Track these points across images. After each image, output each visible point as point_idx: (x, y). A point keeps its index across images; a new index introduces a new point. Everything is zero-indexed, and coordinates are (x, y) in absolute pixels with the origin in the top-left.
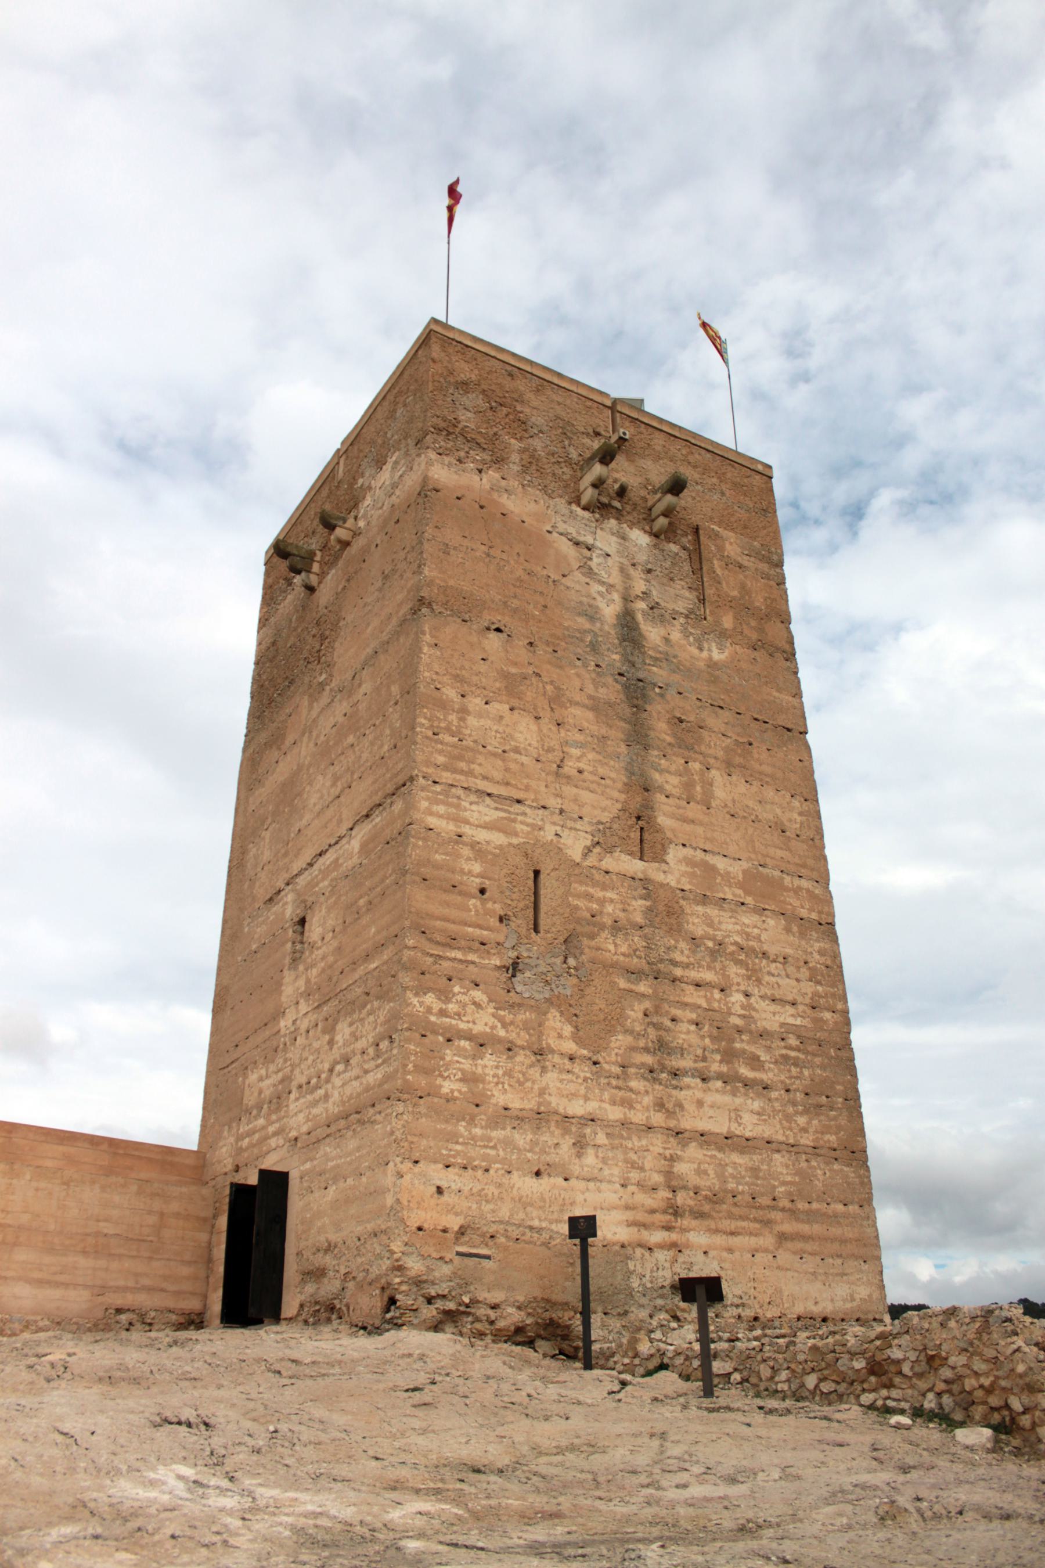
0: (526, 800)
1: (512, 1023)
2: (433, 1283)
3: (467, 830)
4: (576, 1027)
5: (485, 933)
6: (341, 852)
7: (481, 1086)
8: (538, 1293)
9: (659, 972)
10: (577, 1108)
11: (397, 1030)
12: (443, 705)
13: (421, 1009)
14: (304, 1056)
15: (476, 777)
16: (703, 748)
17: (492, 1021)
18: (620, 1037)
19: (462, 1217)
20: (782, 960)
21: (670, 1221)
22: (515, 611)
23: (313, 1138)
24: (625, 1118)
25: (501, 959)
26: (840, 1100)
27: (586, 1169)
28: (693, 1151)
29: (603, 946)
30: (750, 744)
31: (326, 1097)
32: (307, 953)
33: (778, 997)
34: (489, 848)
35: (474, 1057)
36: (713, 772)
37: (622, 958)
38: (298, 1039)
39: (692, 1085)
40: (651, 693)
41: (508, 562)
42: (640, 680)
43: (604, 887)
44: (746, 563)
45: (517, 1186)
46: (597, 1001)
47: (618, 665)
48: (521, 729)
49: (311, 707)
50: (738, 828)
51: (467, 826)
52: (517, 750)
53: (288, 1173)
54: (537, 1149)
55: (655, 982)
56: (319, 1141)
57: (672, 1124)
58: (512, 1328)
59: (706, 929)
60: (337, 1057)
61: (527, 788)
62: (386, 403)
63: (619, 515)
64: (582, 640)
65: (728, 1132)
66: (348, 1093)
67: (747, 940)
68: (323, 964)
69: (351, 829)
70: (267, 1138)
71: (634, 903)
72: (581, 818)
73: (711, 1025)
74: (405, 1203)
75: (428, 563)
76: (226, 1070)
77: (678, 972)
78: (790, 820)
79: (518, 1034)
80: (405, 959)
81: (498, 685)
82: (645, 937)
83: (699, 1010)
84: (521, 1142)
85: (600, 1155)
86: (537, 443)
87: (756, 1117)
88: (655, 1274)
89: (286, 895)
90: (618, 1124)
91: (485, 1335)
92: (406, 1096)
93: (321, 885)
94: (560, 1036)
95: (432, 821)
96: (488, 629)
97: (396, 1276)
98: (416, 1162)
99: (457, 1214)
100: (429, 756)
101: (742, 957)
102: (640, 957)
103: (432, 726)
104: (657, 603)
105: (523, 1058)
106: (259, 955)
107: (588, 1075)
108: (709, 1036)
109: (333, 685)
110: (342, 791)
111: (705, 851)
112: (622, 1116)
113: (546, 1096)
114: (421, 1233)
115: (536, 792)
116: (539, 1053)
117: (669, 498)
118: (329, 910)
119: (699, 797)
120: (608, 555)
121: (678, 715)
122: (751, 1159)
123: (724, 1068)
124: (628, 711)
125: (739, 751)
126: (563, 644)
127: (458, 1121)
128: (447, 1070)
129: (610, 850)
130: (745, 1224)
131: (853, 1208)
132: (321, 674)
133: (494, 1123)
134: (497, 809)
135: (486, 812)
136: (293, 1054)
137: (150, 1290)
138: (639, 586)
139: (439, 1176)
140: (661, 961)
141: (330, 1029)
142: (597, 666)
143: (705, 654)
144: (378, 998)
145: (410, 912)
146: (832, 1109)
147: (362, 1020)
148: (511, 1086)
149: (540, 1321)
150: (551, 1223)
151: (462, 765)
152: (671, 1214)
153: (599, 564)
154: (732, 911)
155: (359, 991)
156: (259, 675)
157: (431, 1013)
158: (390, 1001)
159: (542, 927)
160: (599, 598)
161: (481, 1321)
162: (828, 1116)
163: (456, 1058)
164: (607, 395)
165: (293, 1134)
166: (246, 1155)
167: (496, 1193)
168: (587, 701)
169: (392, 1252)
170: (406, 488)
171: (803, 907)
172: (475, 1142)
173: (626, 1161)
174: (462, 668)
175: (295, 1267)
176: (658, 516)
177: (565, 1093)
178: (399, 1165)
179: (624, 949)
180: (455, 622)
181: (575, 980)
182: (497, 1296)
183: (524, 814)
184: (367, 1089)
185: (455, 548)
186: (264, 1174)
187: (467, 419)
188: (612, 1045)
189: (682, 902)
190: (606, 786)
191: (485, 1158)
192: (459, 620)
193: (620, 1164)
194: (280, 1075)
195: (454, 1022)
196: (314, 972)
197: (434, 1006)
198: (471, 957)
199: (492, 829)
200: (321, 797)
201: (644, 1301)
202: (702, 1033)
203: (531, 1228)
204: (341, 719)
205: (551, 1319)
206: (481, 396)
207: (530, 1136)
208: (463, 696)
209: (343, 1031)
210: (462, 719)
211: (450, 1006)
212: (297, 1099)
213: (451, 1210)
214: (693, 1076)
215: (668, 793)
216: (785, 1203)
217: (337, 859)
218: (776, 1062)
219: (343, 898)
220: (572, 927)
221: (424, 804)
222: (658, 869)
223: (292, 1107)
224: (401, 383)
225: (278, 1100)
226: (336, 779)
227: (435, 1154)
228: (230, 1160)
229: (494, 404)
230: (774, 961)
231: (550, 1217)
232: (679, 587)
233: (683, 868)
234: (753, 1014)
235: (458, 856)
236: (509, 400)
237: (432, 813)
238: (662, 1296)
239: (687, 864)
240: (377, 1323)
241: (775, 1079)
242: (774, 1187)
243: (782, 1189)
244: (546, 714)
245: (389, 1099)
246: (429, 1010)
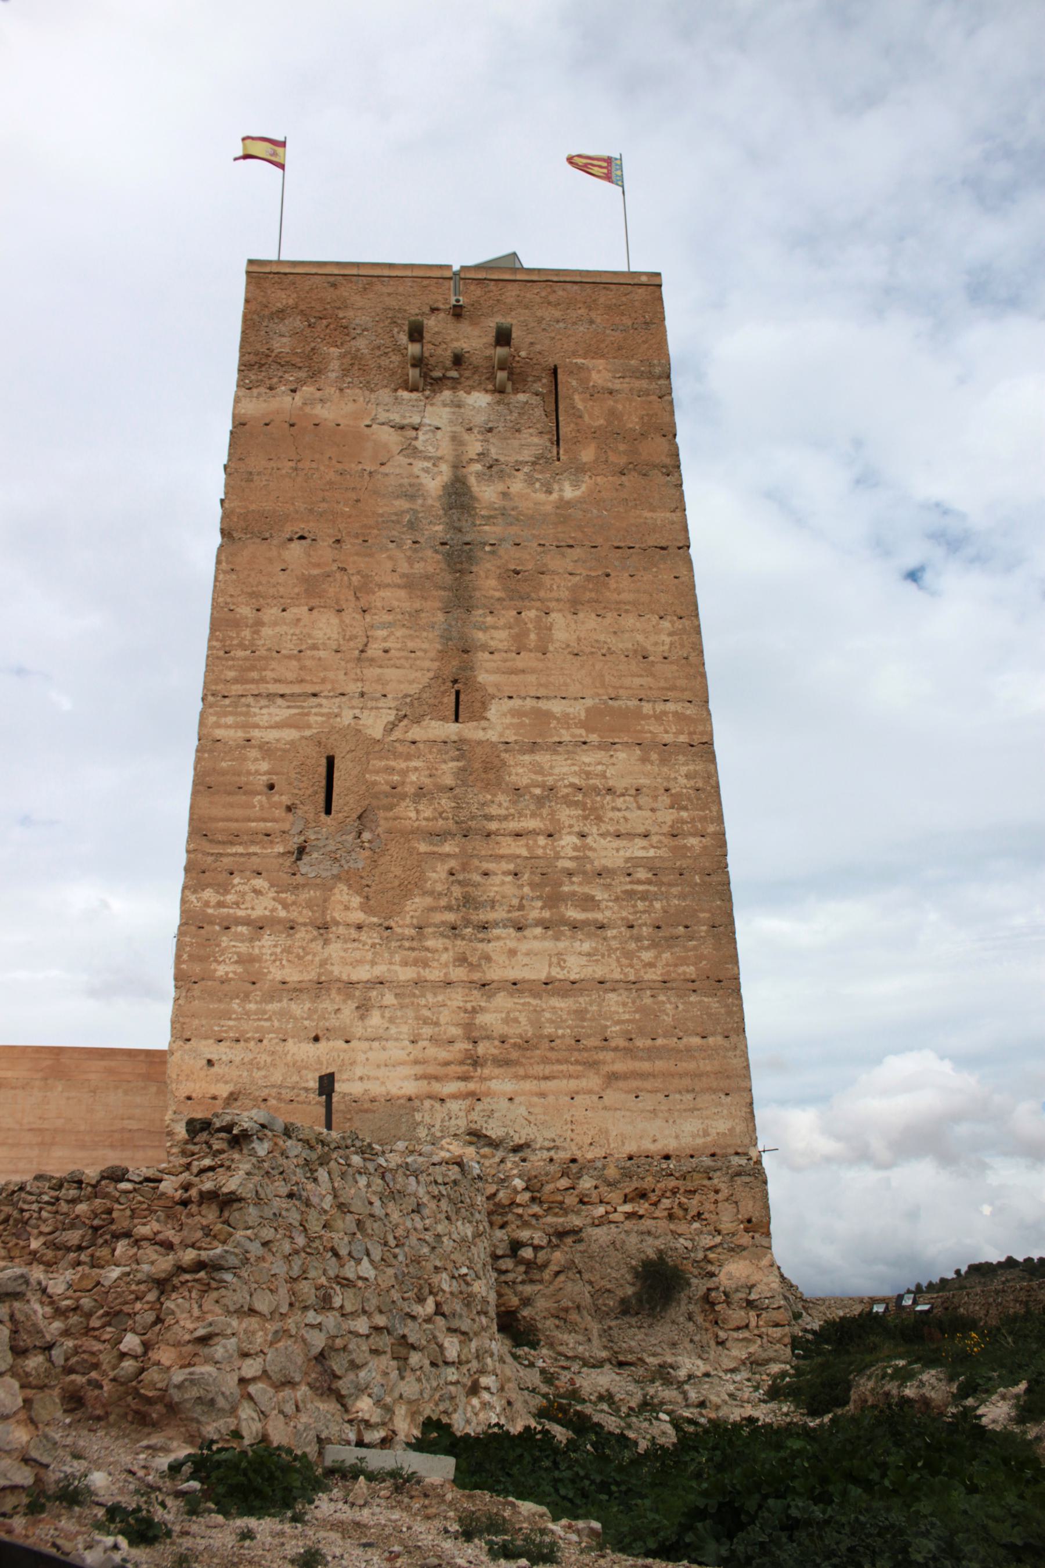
134: (289, 707)
151: (254, 675)
174: (260, 583)
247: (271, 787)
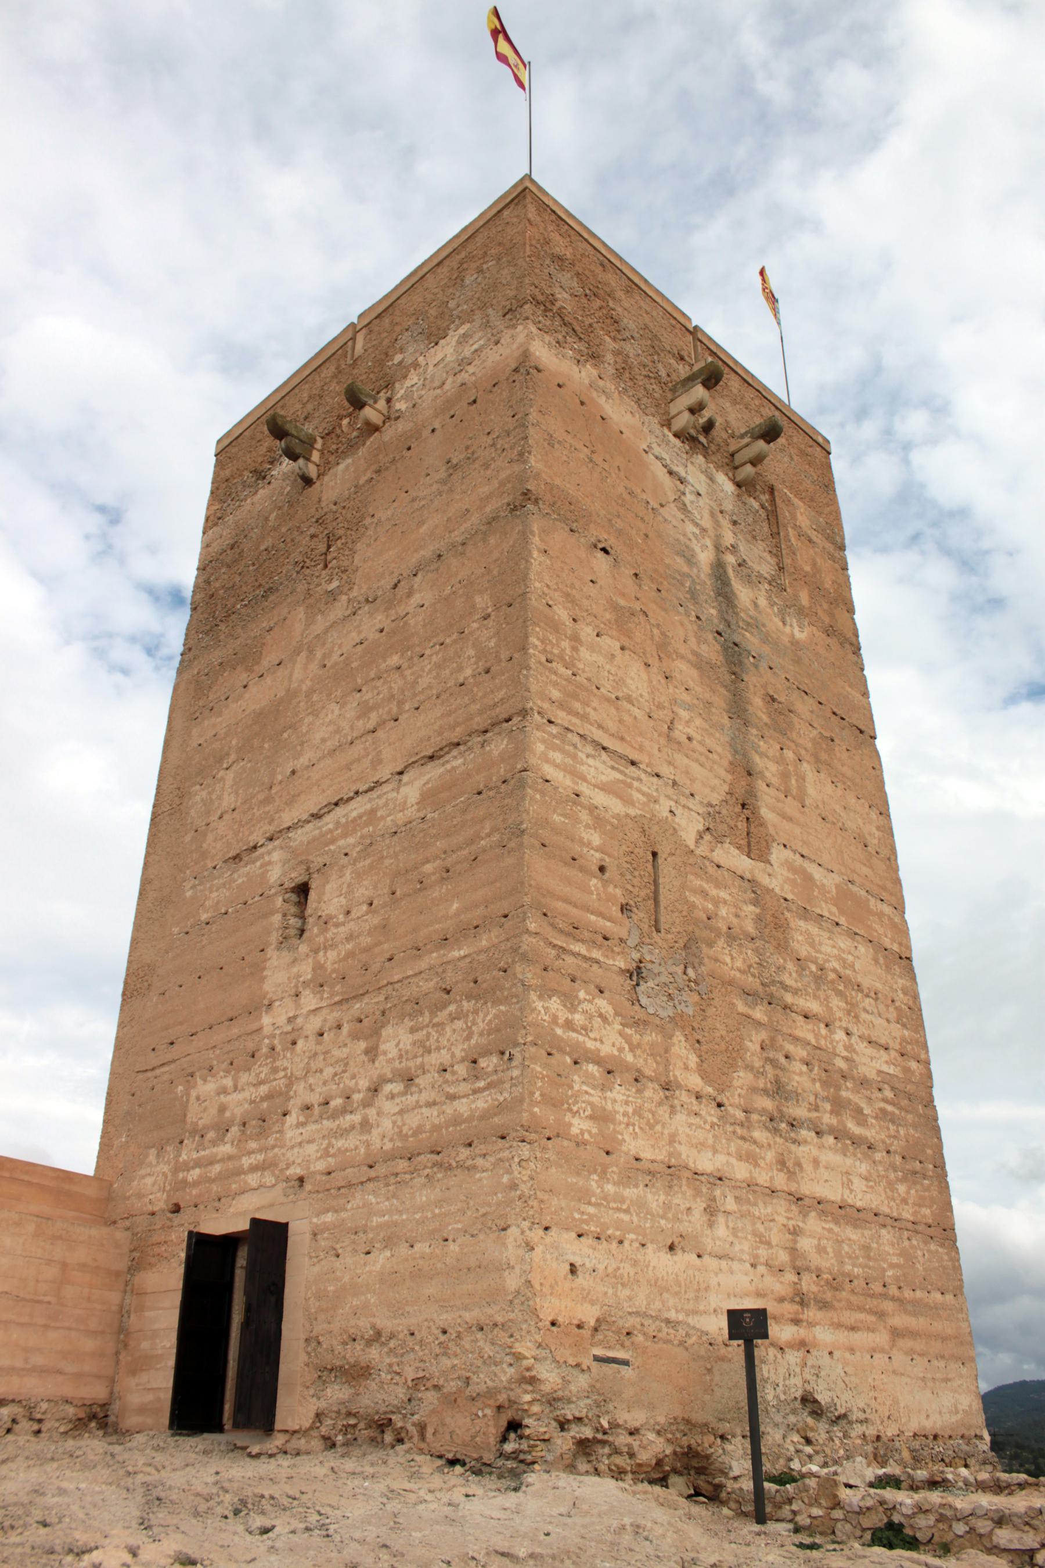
0: (640, 763)
1: (639, 1045)
2: (569, 1401)
3: (583, 788)
4: (699, 1056)
5: (608, 924)
7: (612, 1127)
8: (678, 1412)
9: (771, 995)
10: (706, 1163)
11: (516, 1044)
12: (555, 627)
13: (546, 1018)
14: (314, 1066)
15: (591, 724)
16: (794, 736)
17: (620, 1041)
18: (741, 1074)
19: (598, 1307)
20: (873, 995)
21: (797, 1313)
22: (620, 532)
23: (338, 1178)
24: (751, 1178)
25: (625, 961)
26: (931, 1166)
27: (718, 1243)
28: (813, 1223)
29: (720, 957)
30: (833, 740)
31: (365, 1126)
33: (874, 1039)
34: (608, 816)
35: (604, 1088)
36: (805, 765)
37: (738, 974)
38: (300, 1043)
39: (809, 1139)
40: (746, 661)
41: (610, 473)
42: (736, 644)
43: (718, 885)
44: (814, 539)
45: (652, 1264)
46: (718, 1026)
47: (716, 621)
48: (633, 674)
49: (310, 621)
50: (829, 834)
51: (580, 782)
52: (629, 700)
53: (287, 1224)
54: (670, 1215)
55: (770, 1008)
56: (350, 1185)
57: (793, 1187)
58: (654, 1462)
59: (809, 949)
61: (641, 749)
62: (443, 270)
63: (706, 452)
64: (683, 585)
65: (843, 1200)
67: (844, 967)
69: (401, 773)
70: (239, 1172)
71: (745, 908)
72: (692, 795)
73: (819, 1066)
74: (537, 1287)
75: (534, 452)
76: (149, 1074)
77: (789, 998)
78: (870, 834)
79: (646, 1060)
80: (524, 947)
81: (608, 616)
82: (756, 951)
83: (808, 1047)
84: (654, 1205)
85: (731, 1225)
86: (629, 348)
87: (865, 1183)
88: (787, 1382)
90: (745, 1185)
91: (625, 1472)
92: (533, 1136)
94: (686, 1068)
95: (549, 771)
96: (595, 546)
97: (526, 1392)
98: (546, 1229)
99: (593, 1303)
100: (543, 687)
101: (841, 988)
102: (753, 976)
103: (545, 650)
104: (744, 561)
105: (652, 1092)
106: (214, 927)
107: (715, 1120)
108: (820, 1080)
109: (354, 593)
110: (382, 723)
111: (802, 856)
112: (748, 1175)
113: (676, 1145)
114: (554, 1329)
115: (650, 755)
116: (666, 1087)
117: (761, 444)
118: (359, 876)
119: (794, 792)
120: (699, 494)
121: (772, 693)
122: (863, 1235)
123: (834, 1121)
124: (728, 678)
125: (824, 746)
127: (590, 1173)
128: (575, 1103)
129: (719, 840)
130: (862, 1316)
131: (949, 1297)
132: (331, 581)
133: (626, 1180)
134: (613, 768)
135: (600, 769)
136: (293, 1062)
137: (42, 1371)
138: (729, 538)
139: (582, 1252)
140: (773, 982)
142: (698, 617)
143: (788, 629)
144: (469, 997)
145: (530, 886)
146: (925, 1177)
147: (440, 1026)
148: (641, 1128)
149: (678, 1449)
150: (688, 1315)
152: (798, 1303)
153: (692, 502)
154: (830, 931)
155: (427, 985)
156: (208, 582)
157: (557, 1024)
158: (497, 1002)
159: (663, 926)
160: (694, 541)
161: (620, 1453)
162: (922, 1185)
163: (585, 1088)
164: (689, 319)
167: (632, 1274)
168: (690, 657)
169: (519, 1357)
170: (489, 363)
171: (886, 936)
172: (608, 1203)
173: (755, 1233)
174: (572, 586)
175: (303, 1358)
176: (744, 464)
177: (694, 1141)
178: (528, 1232)
179: (739, 964)
180: (563, 528)
181: (697, 998)
182: (635, 1418)
183: (639, 780)
185: (559, 442)
187: (563, 298)
188: (735, 1083)
189: (787, 915)
190: (714, 762)
191: (619, 1224)
192: (567, 529)
193: (749, 1237)
195: (581, 1038)
196: (332, 955)
197: (560, 1014)
198: (596, 954)
200: (338, 731)
201: (778, 1418)
202: (813, 1076)
203: (668, 1321)
204: (372, 635)
205: (689, 1447)
206: (575, 279)
207: (662, 1198)
208: (574, 620)
209: (397, 1039)
210: (575, 649)
211: (577, 1016)
212: (300, 1125)
213: (586, 1297)
214: (809, 1129)
215: (768, 781)
216: (893, 1290)
218: (876, 1118)
219: (387, 862)
220: (690, 928)
221: (540, 747)
222: (764, 870)
224: (470, 247)
225: (262, 1122)
226: (365, 710)
227: (567, 1218)
229: (588, 292)
230: (867, 996)
231: (686, 1307)
232: (761, 548)
233: (785, 873)
234: (855, 1056)
235: (577, 821)
236: (602, 292)
237: (547, 759)
238: (794, 1412)
239: (789, 870)
240: (488, 1457)
241: (878, 1137)
242: (884, 1270)
243: (890, 1273)
244: (654, 661)
245: (503, 1138)
246: (555, 1019)
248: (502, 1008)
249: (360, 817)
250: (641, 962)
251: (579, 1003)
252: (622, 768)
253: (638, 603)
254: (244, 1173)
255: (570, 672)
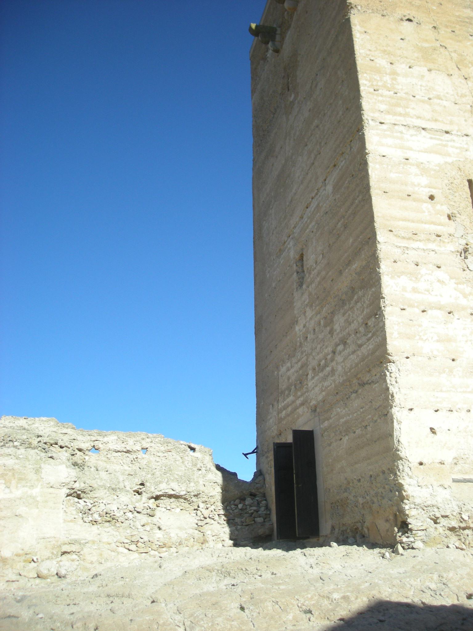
0: (452, 131)
3: (409, 154)
6: (320, 199)
12: (378, 71)
15: (412, 118)
31: (333, 371)
32: (307, 275)
52: (439, 97)
60: (337, 340)
61: (451, 123)
66: (348, 366)
68: (318, 279)
81: (416, 55)
89: (289, 244)
93: (310, 226)
96: (402, 20)
103: (372, 85)
110: (316, 156)
126: (457, 26)
134: (431, 138)
135: (424, 141)
136: (307, 348)
141: (329, 321)
151: (400, 110)
165: (313, 402)
166: (284, 422)
174: (388, 45)
184: (363, 360)
186: (296, 433)
194: (300, 364)
199: (430, 152)
209: (339, 321)
217: (318, 204)
223: (310, 384)
225: (301, 382)
228: (275, 427)
247: (432, 198)
248: (373, 289)
249: (315, 210)
250: (467, 244)
251: (421, 277)
252: (438, 137)
253: (438, 42)
254: (298, 408)
255: (392, 93)
